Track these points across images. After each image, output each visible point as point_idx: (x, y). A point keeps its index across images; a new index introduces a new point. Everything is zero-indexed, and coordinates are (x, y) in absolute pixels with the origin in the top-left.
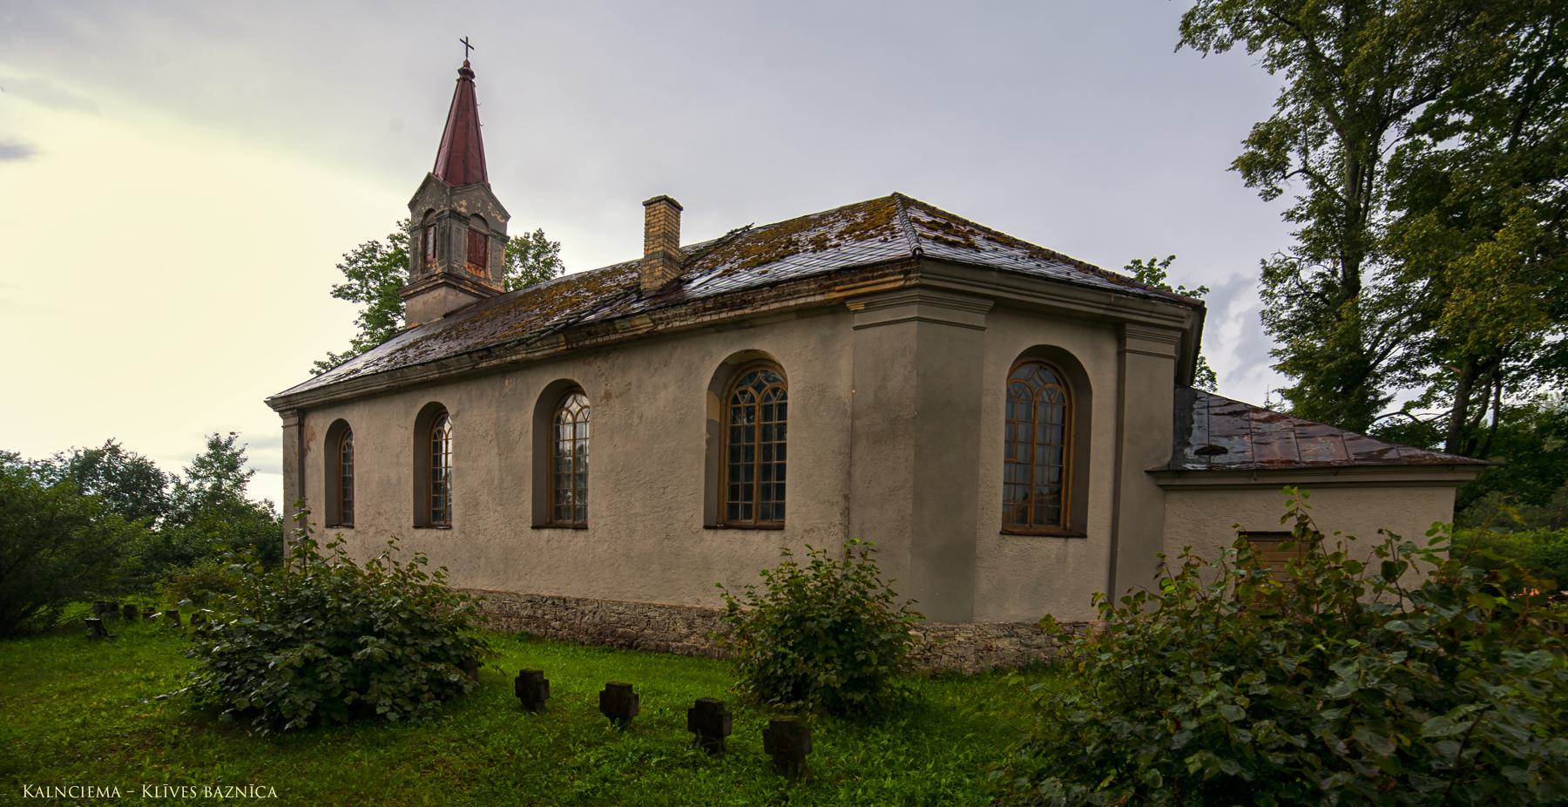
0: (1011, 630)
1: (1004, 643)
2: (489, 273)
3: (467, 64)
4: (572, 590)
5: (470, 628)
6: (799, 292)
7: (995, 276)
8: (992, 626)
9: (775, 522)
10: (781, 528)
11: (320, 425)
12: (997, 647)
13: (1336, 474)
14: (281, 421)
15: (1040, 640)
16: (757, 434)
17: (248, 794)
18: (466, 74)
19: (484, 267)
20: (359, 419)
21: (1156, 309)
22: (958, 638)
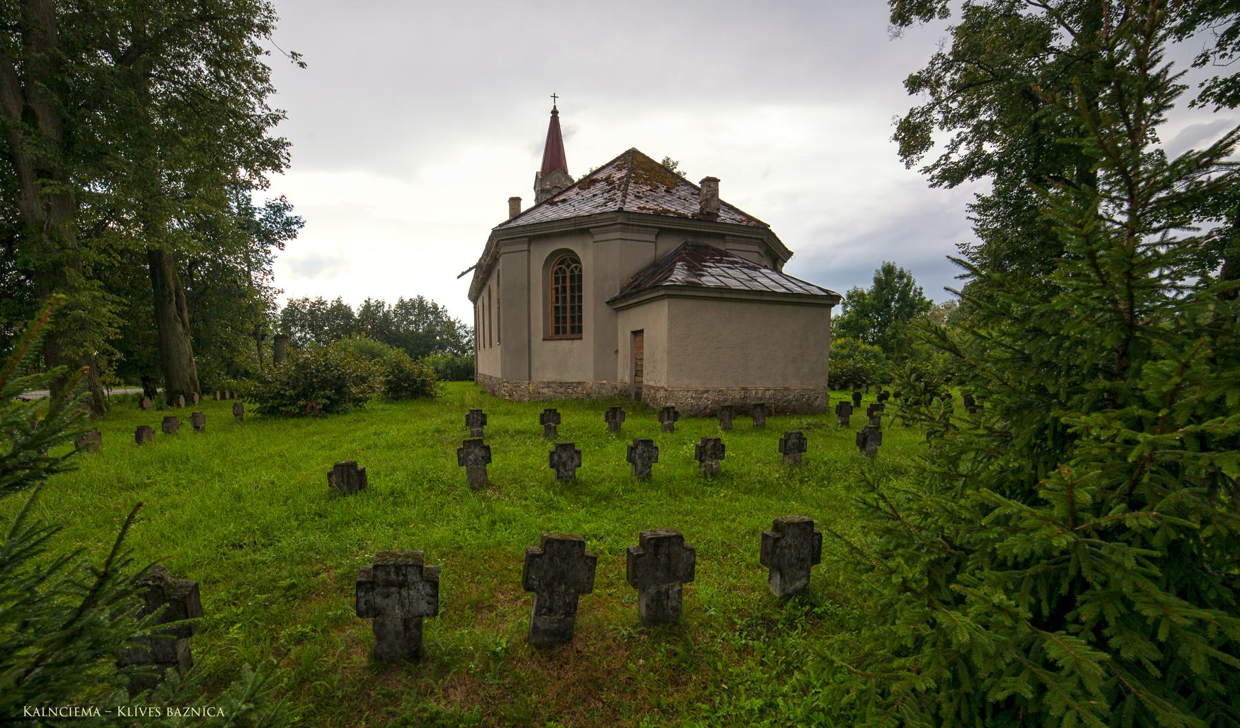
0: (548, 385)
1: (545, 390)
5: (1045, 503)
7: (520, 229)
9: (579, 335)
10: (581, 339)
15: (562, 390)
17: (201, 714)
18: (555, 113)
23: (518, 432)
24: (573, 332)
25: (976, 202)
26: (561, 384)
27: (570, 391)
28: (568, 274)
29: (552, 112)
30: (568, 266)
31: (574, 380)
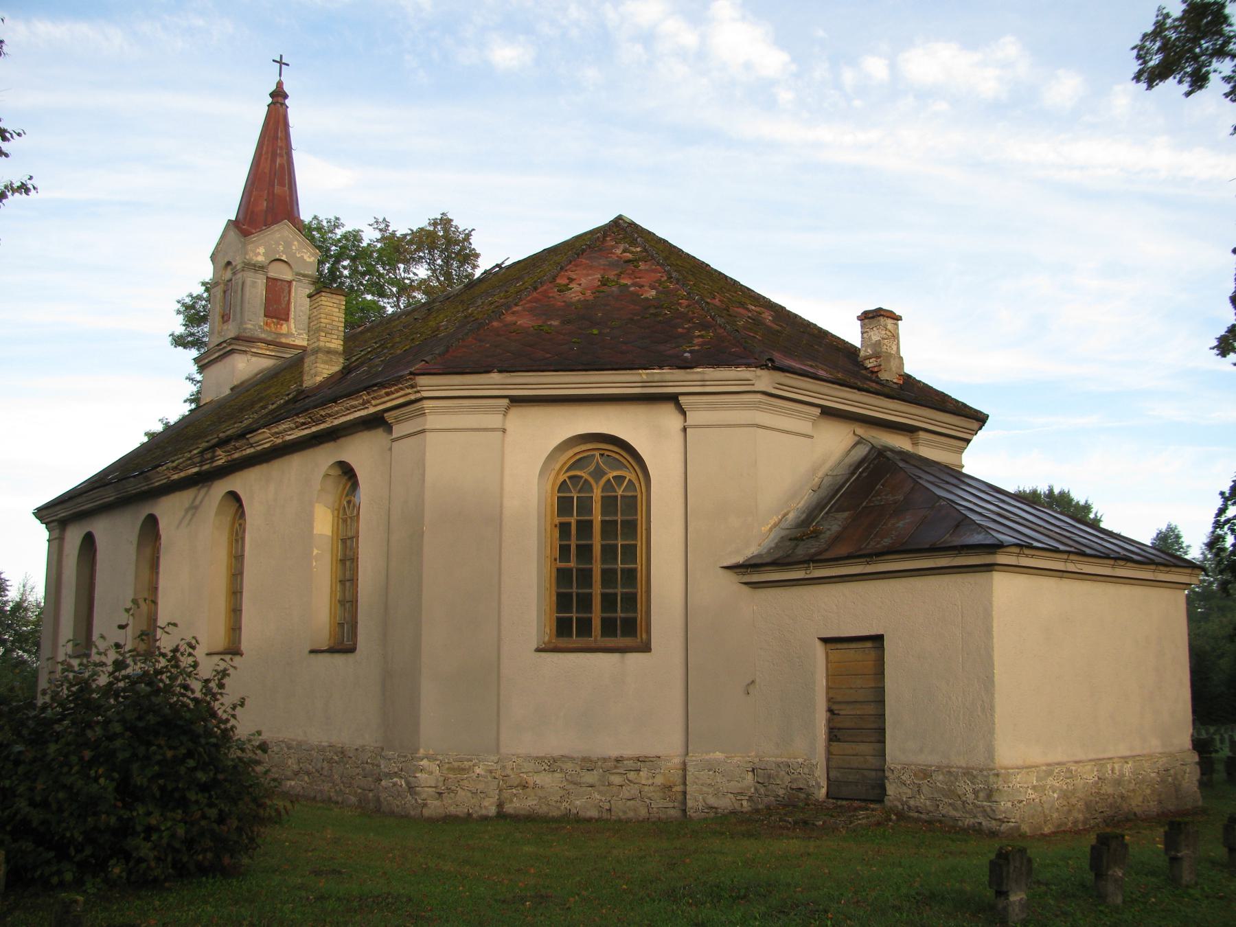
0: (552, 764)
2: (292, 326)
3: (280, 84)
4: (997, 725)
6: (401, 377)
8: (528, 758)
11: (74, 536)
12: (535, 784)
13: (759, 572)
14: (48, 533)
15: (590, 778)
16: (597, 507)
18: (279, 95)
19: (287, 320)
20: (101, 528)
21: (707, 377)
22: (478, 771)
23: (962, 616)
24: (609, 628)
25: (1099, 515)
26: (588, 764)
27: (616, 780)
28: (597, 494)
29: (272, 95)
30: (598, 473)
31: (628, 752)
